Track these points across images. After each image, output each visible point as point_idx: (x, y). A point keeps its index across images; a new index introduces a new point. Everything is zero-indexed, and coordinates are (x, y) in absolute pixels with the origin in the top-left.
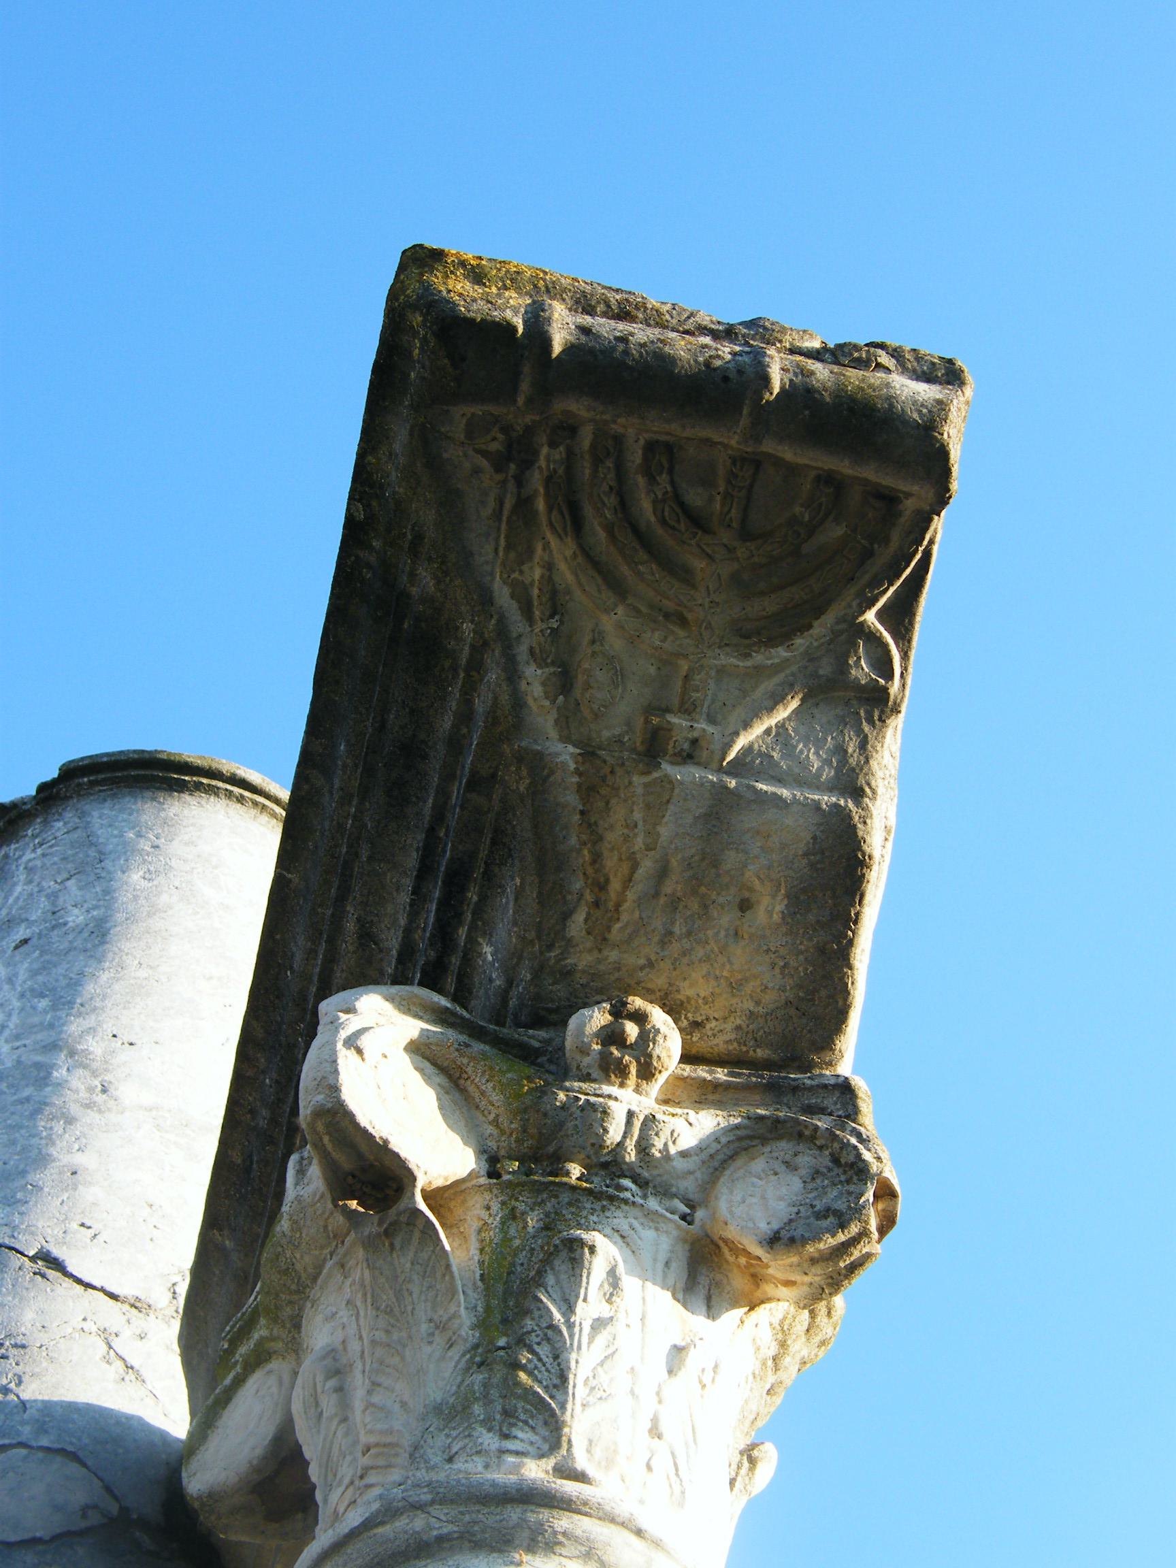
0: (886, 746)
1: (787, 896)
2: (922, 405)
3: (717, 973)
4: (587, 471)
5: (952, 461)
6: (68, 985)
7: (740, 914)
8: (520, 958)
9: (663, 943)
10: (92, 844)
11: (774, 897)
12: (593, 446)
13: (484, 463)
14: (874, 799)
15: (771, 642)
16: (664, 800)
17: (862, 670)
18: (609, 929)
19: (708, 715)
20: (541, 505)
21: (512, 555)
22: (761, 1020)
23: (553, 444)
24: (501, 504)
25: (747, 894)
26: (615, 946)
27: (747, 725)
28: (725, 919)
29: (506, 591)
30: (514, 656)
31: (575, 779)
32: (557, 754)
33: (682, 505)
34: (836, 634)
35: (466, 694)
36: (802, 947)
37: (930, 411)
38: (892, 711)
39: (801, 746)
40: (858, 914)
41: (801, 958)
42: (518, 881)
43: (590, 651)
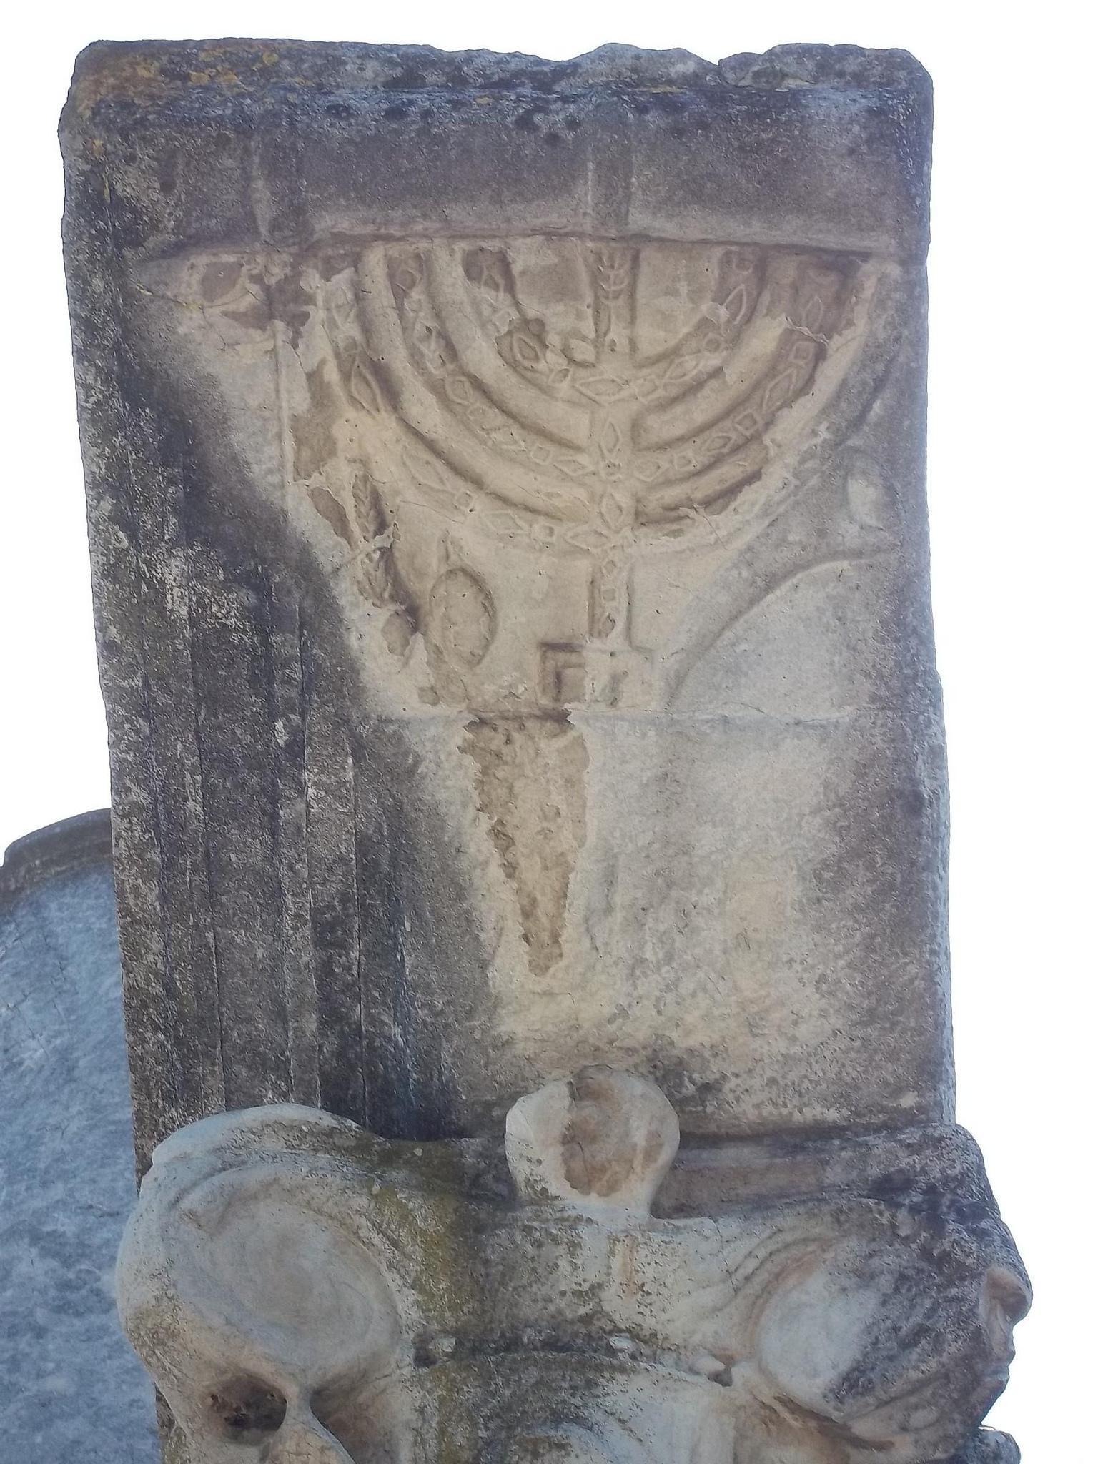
6: (27, 1147)
10: (49, 948)
21: (306, 454)
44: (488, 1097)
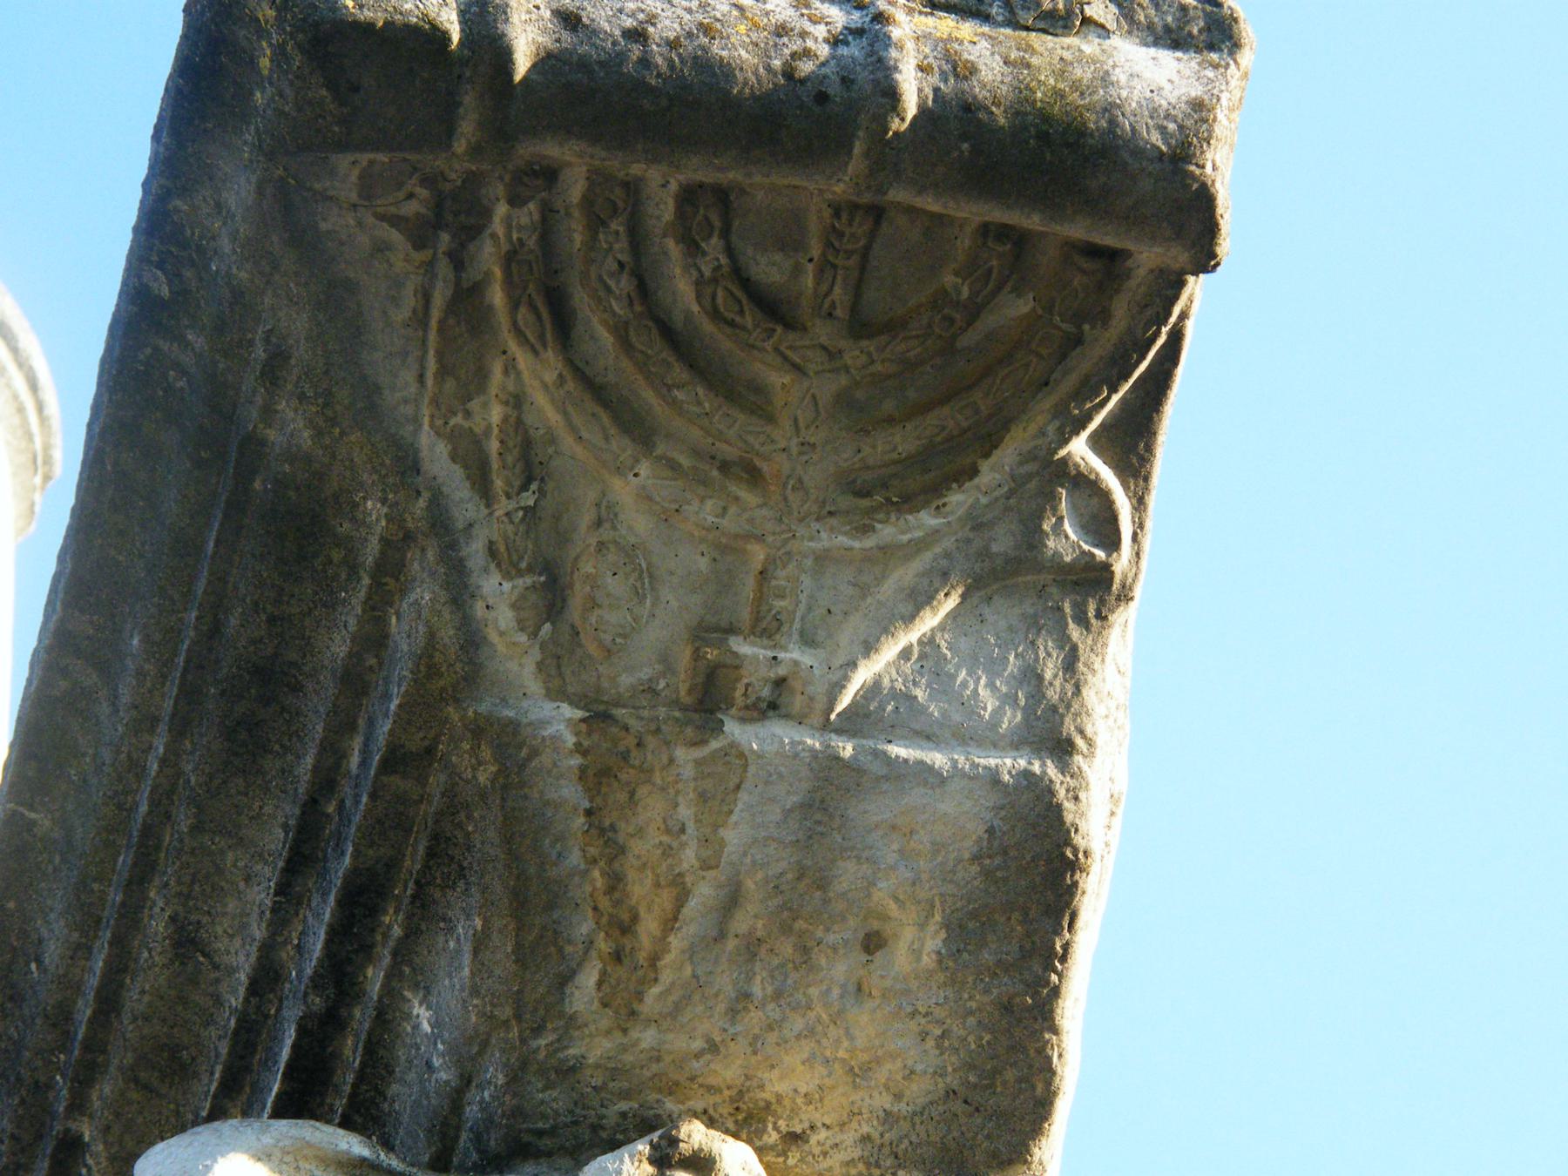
0: (1108, 659)
1: (947, 925)
2: (1168, 116)
3: (828, 1053)
4: (578, 238)
5: (1219, 211)
7: (864, 957)
8: (485, 1044)
9: (733, 1013)
11: (922, 926)
12: (588, 202)
13: (395, 236)
14: (1090, 755)
15: (908, 502)
16: (731, 785)
17: (1067, 537)
18: (639, 996)
19: (802, 633)
20: (497, 296)
21: (450, 384)
22: (905, 1126)
23: (515, 201)
24: (427, 299)
25: (875, 925)
26: (649, 1021)
27: (869, 648)
28: (840, 969)
29: (442, 449)
30: (461, 560)
31: (576, 761)
32: (543, 723)
33: (746, 283)
34: (1018, 483)
35: (373, 609)
36: (974, 1005)
37: (1181, 127)
38: (1118, 599)
39: (963, 674)
40: (1066, 947)
41: (971, 1021)
42: (478, 923)
43: (593, 541)
44: (540, 1125)
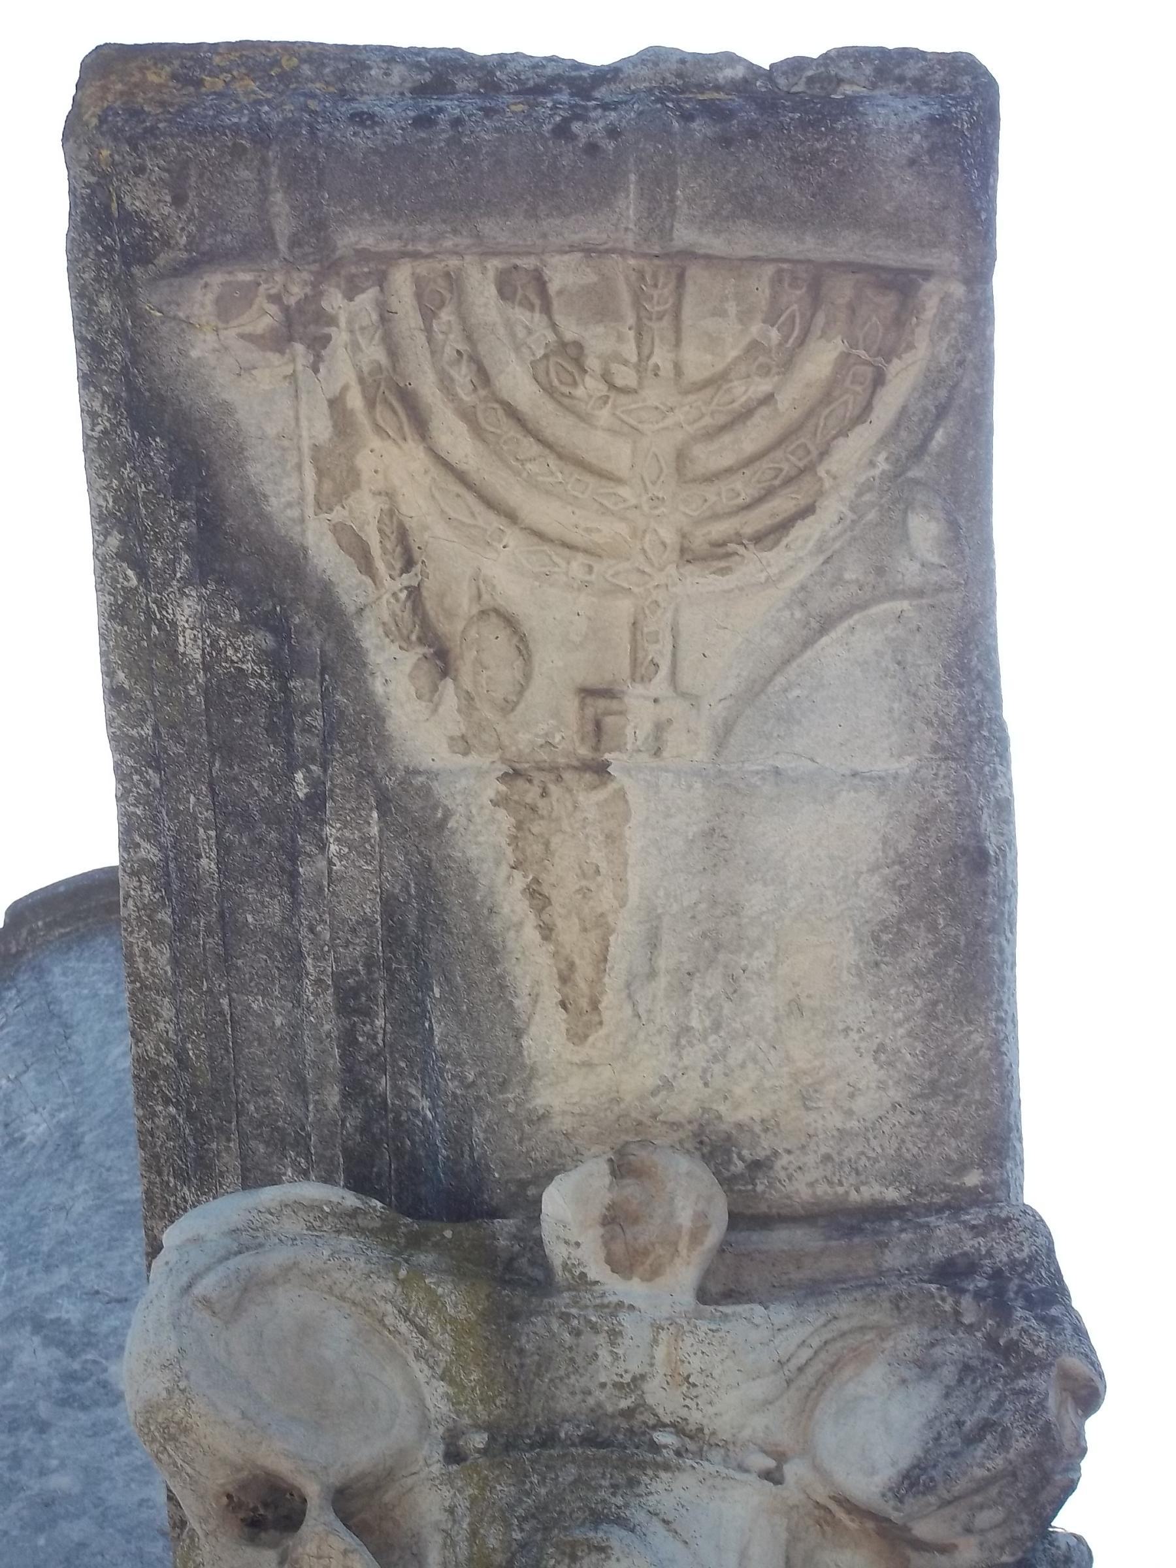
6: (29, 1228)
10: (53, 1015)
